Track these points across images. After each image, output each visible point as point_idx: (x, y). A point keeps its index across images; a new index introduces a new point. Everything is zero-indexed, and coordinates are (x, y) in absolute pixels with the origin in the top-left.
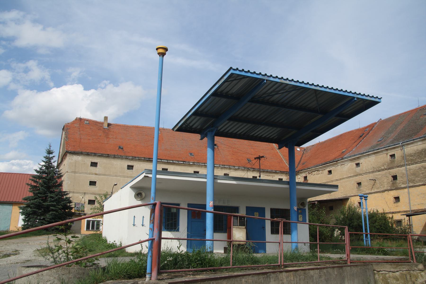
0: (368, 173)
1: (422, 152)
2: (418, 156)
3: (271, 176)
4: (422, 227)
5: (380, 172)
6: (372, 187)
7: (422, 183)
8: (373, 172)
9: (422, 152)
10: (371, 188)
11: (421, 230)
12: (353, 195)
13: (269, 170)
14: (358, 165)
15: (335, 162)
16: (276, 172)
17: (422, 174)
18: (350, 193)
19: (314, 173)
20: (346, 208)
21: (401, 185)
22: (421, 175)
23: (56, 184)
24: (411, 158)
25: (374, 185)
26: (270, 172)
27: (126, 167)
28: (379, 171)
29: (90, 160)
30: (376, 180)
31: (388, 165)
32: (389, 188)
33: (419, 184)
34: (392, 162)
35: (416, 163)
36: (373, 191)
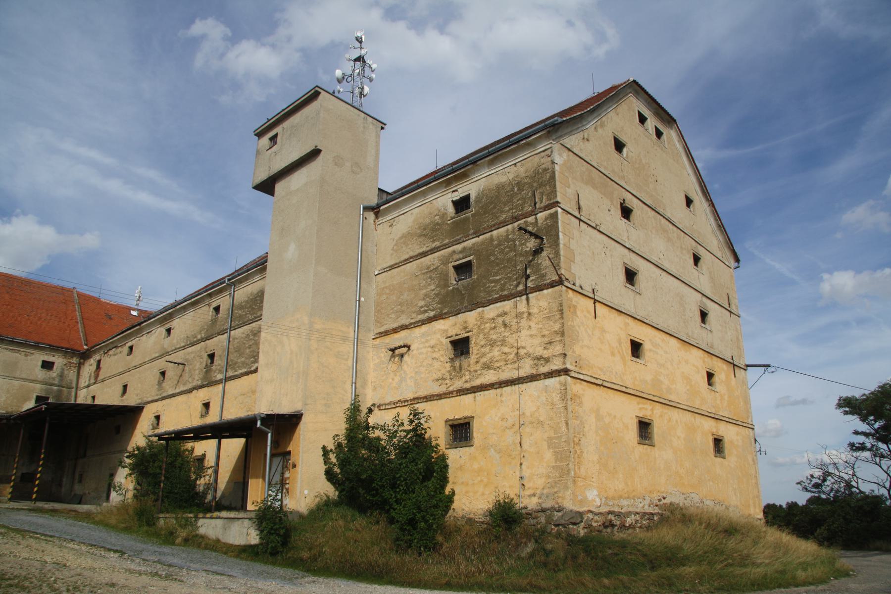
0: (179, 348)
1: (257, 297)
2: (250, 307)
3: (23, 354)
4: (230, 473)
5: (193, 347)
6: (178, 382)
7: (246, 370)
8: (184, 348)
9: (257, 297)
10: (176, 382)
11: (227, 479)
12: (150, 399)
13: (19, 339)
14: (169, 331)
15: (138, 327)
16: (38, 346)
17: (249, 348)
18: (148, 395)
19: (111, 352)
20: (388, 454)
21: (216, 376)
22: (248, 351)
23: (885, 504)
24: (240, 312)
25: (181, 376)
26: (19, 344)
27: (40, 364)
28: (193, 344)
29: (40, 357)
30: (185, 365)
31: (207, 331)
32: (199, 383)
33: (241, 371)
34: (214, 321)
35: (245, 324)
36: (177, 391)
